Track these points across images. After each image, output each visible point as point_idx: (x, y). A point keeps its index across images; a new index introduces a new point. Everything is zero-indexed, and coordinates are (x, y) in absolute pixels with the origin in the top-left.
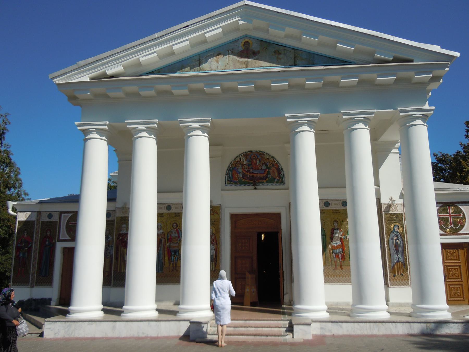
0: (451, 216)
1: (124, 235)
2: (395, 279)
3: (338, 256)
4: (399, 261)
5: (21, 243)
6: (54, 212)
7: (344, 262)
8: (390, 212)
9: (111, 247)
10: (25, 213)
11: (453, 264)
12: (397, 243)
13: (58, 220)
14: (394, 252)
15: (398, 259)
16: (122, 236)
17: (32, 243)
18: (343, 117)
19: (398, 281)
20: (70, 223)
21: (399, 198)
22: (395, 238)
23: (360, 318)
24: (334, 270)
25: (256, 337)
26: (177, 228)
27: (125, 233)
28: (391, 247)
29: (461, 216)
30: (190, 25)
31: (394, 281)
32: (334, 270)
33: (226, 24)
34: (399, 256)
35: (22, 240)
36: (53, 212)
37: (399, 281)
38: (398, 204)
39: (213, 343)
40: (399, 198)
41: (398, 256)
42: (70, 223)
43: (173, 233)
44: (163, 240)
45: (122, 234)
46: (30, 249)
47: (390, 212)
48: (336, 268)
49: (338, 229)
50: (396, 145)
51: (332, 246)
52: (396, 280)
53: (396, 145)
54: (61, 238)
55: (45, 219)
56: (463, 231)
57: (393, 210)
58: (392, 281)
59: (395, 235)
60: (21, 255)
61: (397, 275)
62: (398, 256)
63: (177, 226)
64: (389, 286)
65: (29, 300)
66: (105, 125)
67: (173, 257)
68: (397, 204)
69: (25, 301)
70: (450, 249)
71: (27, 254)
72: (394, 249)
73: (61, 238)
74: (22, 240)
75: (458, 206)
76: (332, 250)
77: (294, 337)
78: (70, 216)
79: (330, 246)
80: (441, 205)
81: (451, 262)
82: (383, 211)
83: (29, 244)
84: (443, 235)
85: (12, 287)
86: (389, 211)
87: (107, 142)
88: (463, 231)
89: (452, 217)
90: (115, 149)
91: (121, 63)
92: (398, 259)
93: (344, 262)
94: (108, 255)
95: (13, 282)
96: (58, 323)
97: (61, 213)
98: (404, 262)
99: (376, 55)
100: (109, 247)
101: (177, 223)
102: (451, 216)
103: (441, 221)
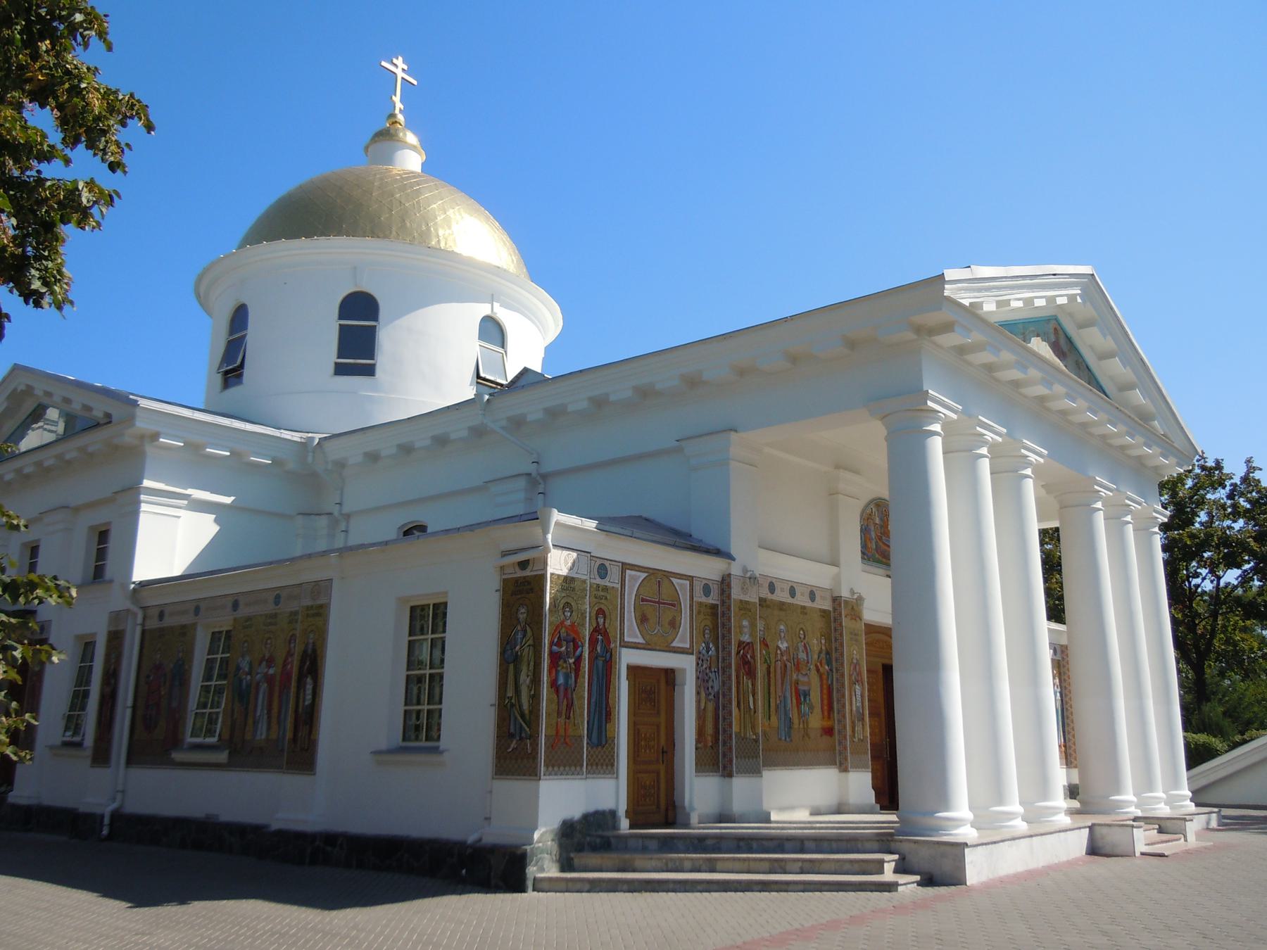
1: (746, 645)
5: (559, 644)
6: (611, 563)
9: (714, 673)
10: (566, 553)
16: (744, 648)
23: (1158, 811)
25: (1168, 844)
26: (805, 641)
27: (748, 641)
30: (1059, 274)
36: (609, 562)
39: (1167, 856)
43: (801, 651)
44: (788, 664)
46: (579, 660)
58: (739, 760)
63: (804, 638)
65: (586, 817)
67: (803, 706)
69: (577, 822)
71: (573, 675)
77: (1188, 840)
78: (679, 581)
83: (576, 647)
90: (1043, 483)
94: (710, 694)
95: (547, 765)
96: (979, 847)
97: (625, 566)
99: (1156, 422)
101: (804, 628)
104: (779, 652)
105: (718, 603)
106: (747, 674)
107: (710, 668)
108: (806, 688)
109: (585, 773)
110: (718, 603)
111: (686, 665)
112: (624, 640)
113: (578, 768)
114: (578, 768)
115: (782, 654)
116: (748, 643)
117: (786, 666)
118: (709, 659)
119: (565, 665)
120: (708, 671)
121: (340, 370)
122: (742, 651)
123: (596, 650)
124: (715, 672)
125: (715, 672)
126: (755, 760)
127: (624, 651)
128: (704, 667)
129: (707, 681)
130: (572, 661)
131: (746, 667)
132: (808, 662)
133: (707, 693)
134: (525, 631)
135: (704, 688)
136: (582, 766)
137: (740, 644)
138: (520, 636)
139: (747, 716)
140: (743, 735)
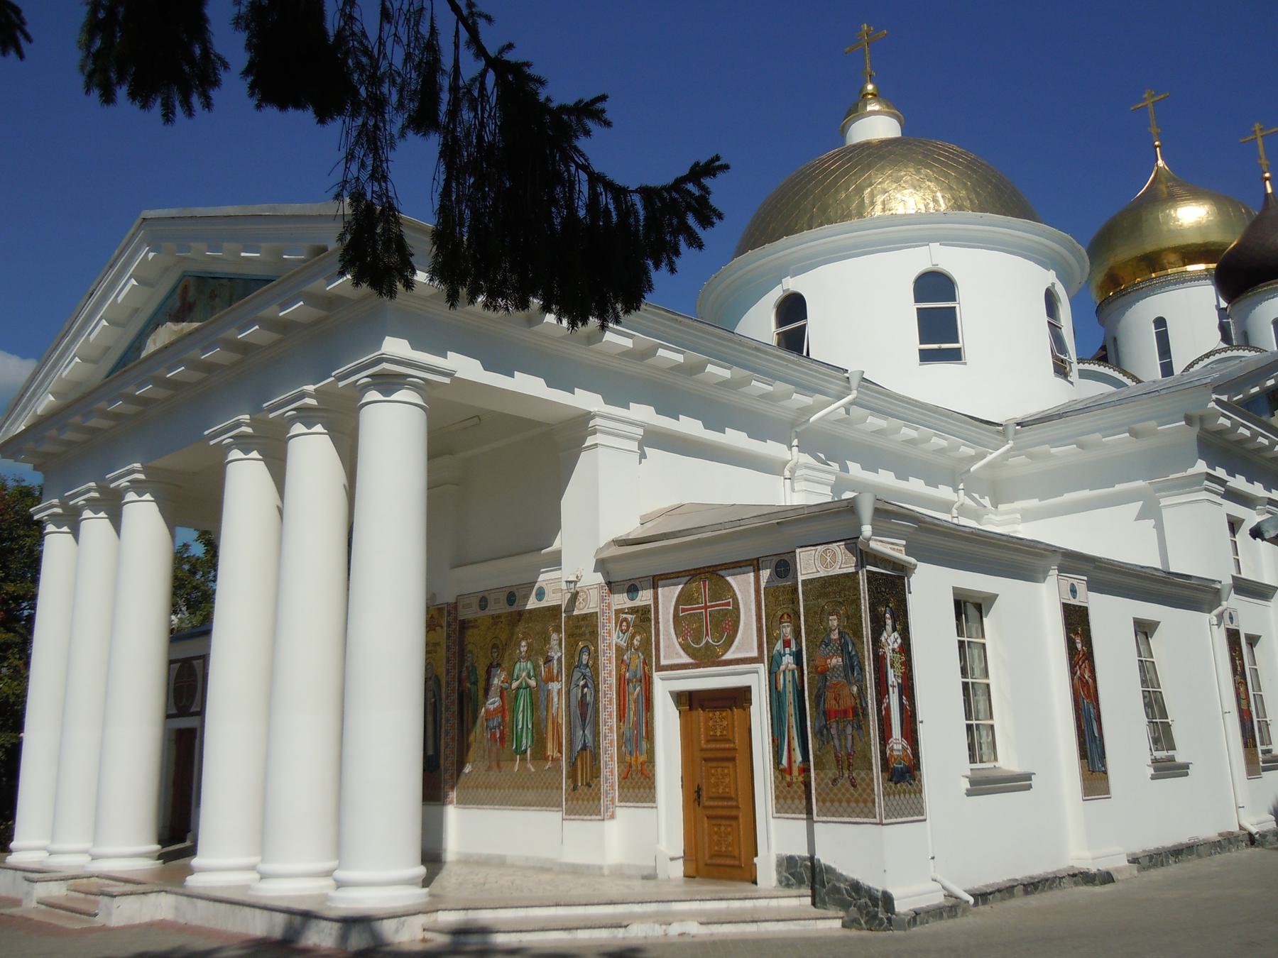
0: (704, 610)
2: (844, 799)
3: (493, 735)
4: (584, 747)
7: (503, 750)
8: (576, 613)
11: (719, 755)
12: (584, 696)
13: (651, 602)
14: (578, 723)
15: (585, 741)
18: (449, 382)
19: (836, 804)
20: (684, 610)
21: (594, 571)
22: (582, 683)
24: (486, 771)
25: (53, 909)
28: (572, 709)
29: (730, 606)
31: (787, 802)
32: (486, 771)
33: (123, 296)
34: (586, 732)
37: (866, 806)
38: (590, 588)
40: (594, 571)
41: (584, 731)
42: (684, 610)
47: (575, 613)
48: (489, 769)
49: (499, 665)
50: (590, 426)
51: (487, 711)
52: (577, 799)
53: (590, 426)
54: (663, 662)
55: (623, 602)
57: (581, 606)
59: (583, 674)
61: (580, 784)
62: (584, 731)
64: (815, 818)
66: (89, 491)
68: (589, 587)
70: (714, 709)
72: (578, 712)
73: (663, 662)
75: (723, 577)
76: (486, 720)
79: (483, 710)
80: (685, 579)
81: (718, 746)
82: (563, 610)
84: (689, 668)
85: (819, 819)
86: (574, 610)
87: (157, 504)
88: (733, 652)
89: (702, 612)
91: (47, 391)
92: (585, 741)
93: (503, 750)
98: (595, 748)
102: (704, 610)
103: (730, 624)
111: (758, 681)
121: (926, 356)
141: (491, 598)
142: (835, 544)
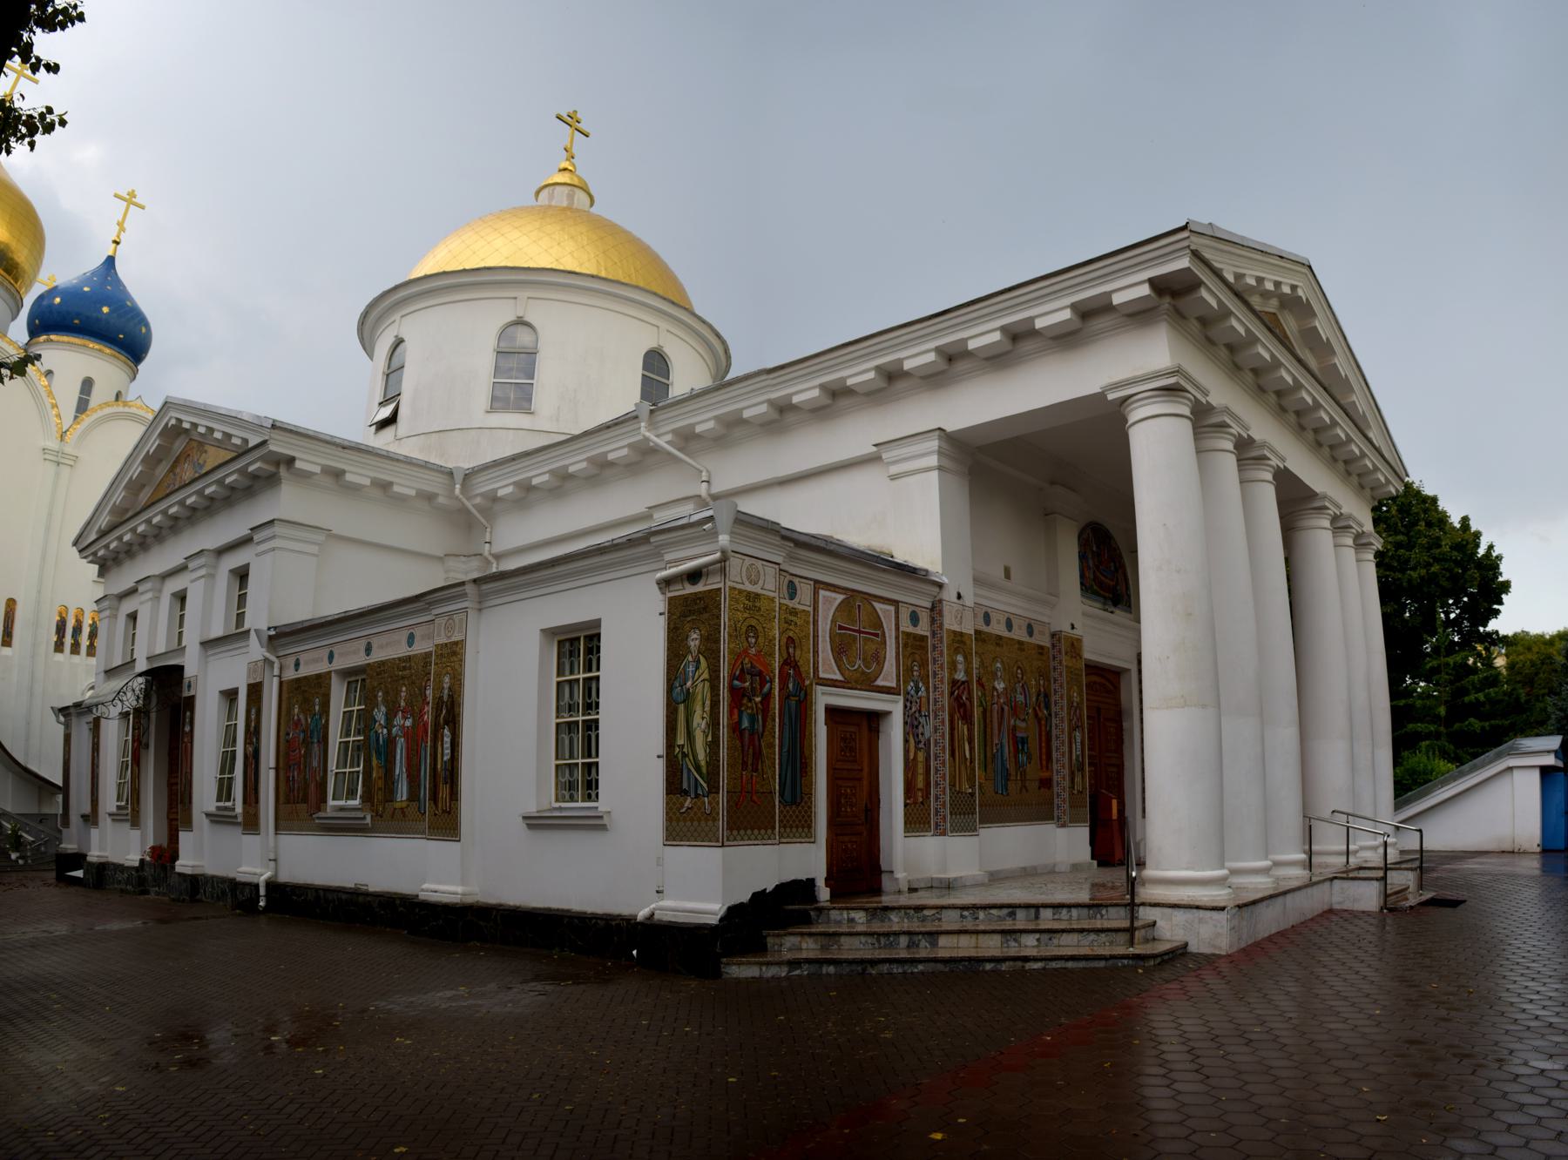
9: (924, 718)
16: (958, 688)
17: (772, 681)
35: (742, 663)
44: (1006, 708)
45: (958, 681)
56: (881, 609)
60: (745, 724)
74: (742, 663)
100: (921, 716)
104: (995, 694)
105: (928, 634)
106: (963, 719)
107: (920, 711)
108: (1024, 735)
109: (777, 837)
110: (928, 634)
111: (896, 708)
112: (818, 675)
113: (769, 831)
114: (769, 831)
115: (998, 696)
116: (963, 683)
117: (1003, 709)
118: (918, 701)
119: (750, 705)
120: (917, 715)
122: (956, 692)
123: (788, 687)
124: (925, 716)
125: (925, 716)
126: (970, 816)
127: (819, 687)
128: (913, 709)
129: (917, 727)
130: (758, 699)
131: (962, 710)
132: (1026, 706)
133: (917, 740)
134: (698, 662)
135: (913, 735)
136: (774, 828)
137: (954, 683)
138: (691, 668)
139: (963, 768)
140: (958, 789)
141: (994, 617)
142: (761, 562)
